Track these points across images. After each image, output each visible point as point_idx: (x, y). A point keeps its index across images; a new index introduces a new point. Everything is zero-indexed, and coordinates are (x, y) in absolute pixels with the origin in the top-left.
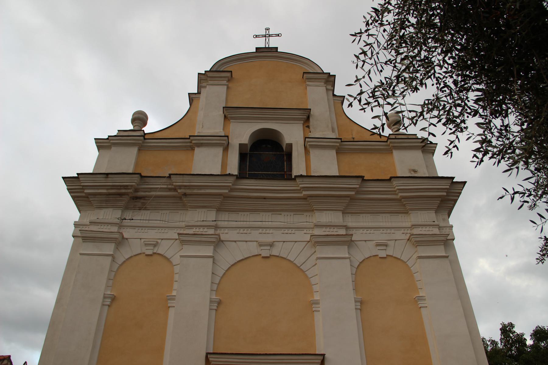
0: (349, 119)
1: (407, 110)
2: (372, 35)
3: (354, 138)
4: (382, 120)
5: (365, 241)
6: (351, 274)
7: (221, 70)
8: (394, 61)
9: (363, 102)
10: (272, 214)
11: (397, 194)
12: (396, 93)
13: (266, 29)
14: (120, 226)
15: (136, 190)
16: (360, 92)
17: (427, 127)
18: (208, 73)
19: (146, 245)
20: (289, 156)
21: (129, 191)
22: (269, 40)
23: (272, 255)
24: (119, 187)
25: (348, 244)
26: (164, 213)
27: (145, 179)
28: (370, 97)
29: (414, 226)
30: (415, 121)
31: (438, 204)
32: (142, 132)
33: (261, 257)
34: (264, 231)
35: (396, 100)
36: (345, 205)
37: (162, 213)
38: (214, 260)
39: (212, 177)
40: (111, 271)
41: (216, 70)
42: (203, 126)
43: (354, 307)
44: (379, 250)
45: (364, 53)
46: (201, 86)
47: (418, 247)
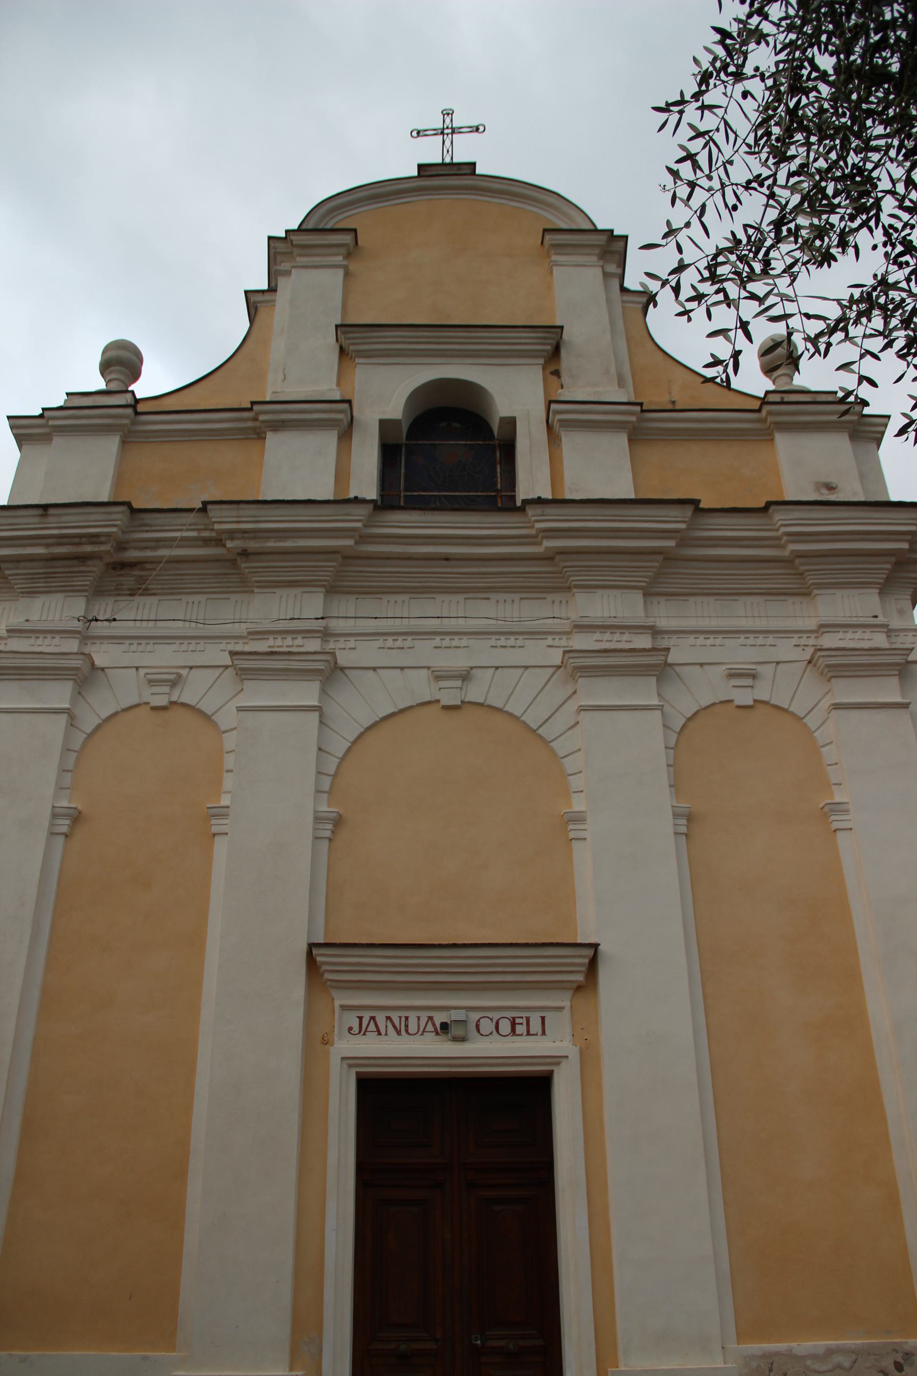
0: (661, 354)
1: (800, 312)
2: (711, 108)
3: (673, 402)
4: (733, 343)
5: (701, 665)
6: (666, 748)
7: (329, 226)
8: (770, 181)
9: (686, 292)
10: (466, 599)
11: (783, 547)
12: (773, 269)
13: (445, 112)
14: (85, 638)
15: (121, 546)
16: (677, 266)
17: (857, 362)
18: (294, 235)
19: (152, 684)
20: (509, 449)
21: (103, 548)
22: (452, 143)
23: (466, 700)
24: (77, 540)
25: (657, 673)
26: (193, 602)
27: (142, 515)
28: (703, 280)
29: (824, 628)
30: (822, 348)
31: (886, 572)
32: (129, 396)
33: (441, 706)
34: (447, 642)
35: (771, 287)
36: (651, 574)
37: (188, 603)
38: (321, 716)
39: (310, 506)
40: (68, 750)
41: (315, 227)
42: (285, 375)
43: (670, 829)
44: (734, 688)
45: (690, 157)
46: (276, 271)
47: (833, 680)
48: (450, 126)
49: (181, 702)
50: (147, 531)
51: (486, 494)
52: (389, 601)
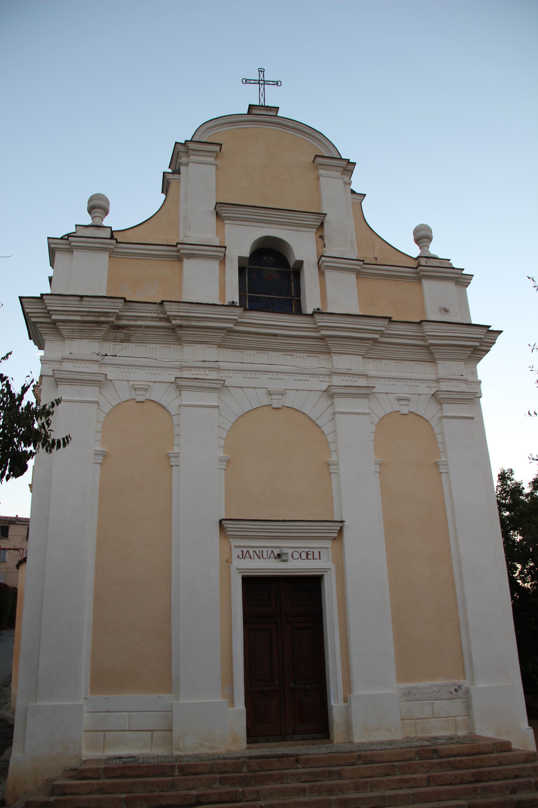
3: (376, 259)
13: (260, 70)
15: (119, 318)
26: (153, 348)
37: (150, 348)
39: (215, 307)
48: (263, 79)
49: (159, 403)
50: (132, 312)
51: (287, 298)
52: (246, 354)
